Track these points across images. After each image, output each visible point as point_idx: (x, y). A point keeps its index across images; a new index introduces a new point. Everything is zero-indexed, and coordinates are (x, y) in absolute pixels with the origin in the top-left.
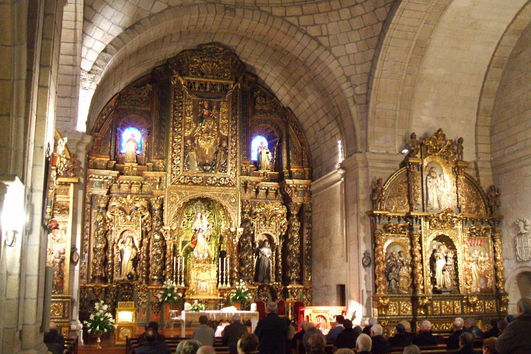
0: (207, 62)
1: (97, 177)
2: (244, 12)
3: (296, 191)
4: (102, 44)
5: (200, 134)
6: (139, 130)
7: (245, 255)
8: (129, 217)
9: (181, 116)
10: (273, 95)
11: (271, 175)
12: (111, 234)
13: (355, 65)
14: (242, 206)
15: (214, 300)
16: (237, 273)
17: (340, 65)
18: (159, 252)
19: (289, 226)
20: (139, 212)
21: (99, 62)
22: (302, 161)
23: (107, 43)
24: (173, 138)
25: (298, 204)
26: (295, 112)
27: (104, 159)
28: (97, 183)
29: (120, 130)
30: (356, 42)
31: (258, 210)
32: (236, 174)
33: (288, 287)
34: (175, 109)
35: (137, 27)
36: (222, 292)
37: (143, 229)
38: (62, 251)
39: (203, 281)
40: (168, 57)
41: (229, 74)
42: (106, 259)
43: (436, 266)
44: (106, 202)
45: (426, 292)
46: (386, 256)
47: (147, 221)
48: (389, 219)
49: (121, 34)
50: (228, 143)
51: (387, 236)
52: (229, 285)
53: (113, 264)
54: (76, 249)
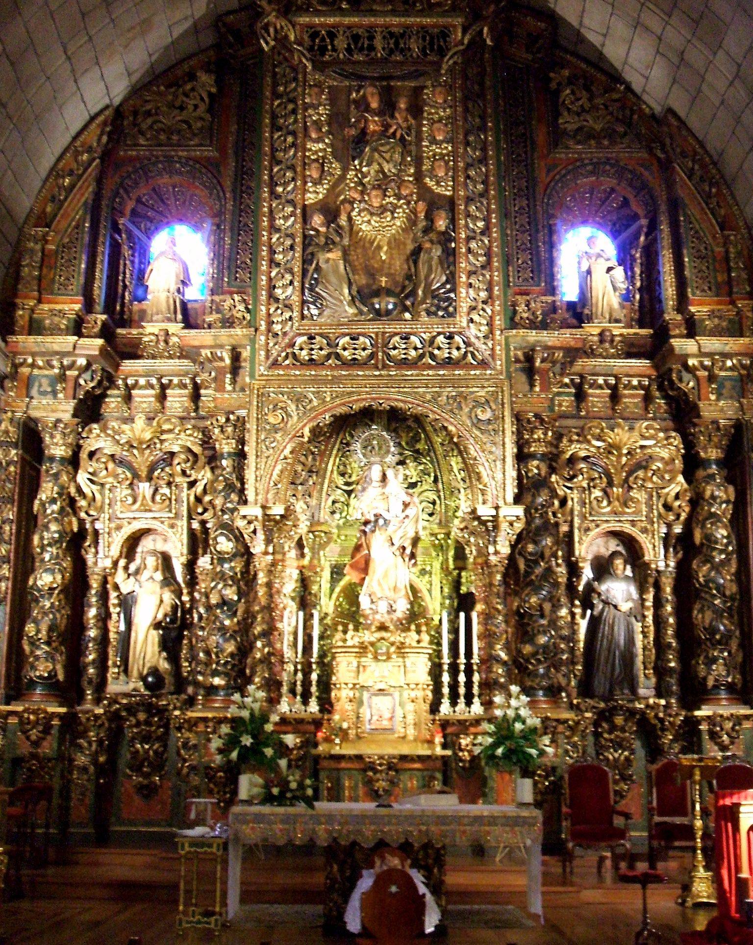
3: (712, 378)
5: (357, 196)
8: (145, 488)
9: (294, 145)
10: (614, 77)
12: (96, 543)
14: (519, 434)
15: (420, 758)
18: (231, 594)
19: (696, 502)
20: (178, 468)
22: (729, 282)
24: (272, 219)
26: (694, 122)
27: (66, 307)
28: (45, 382)
32: (490, 324)
33: (697, 713)
37: (196, 525)
42: (77, 624)
43: (434, 811)
47: (207, 498)
50: (453, 221)
52: (477, 708)
53: (103, 641)
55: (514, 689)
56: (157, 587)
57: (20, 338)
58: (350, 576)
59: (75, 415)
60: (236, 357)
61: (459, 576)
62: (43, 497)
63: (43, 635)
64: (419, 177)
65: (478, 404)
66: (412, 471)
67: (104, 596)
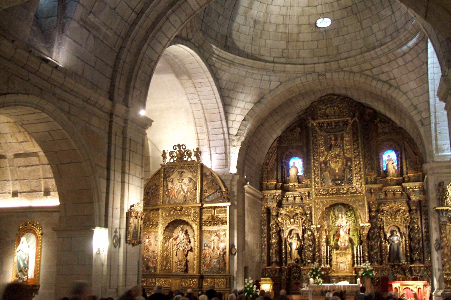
2: (332, 75)
3: (413, 191)
7: (373, 243)
8: (292, 220)
10: (390, 120)
11: (397, 180)
13: (418, 96)
15: (350, 276)
17: (408, 99)
18: (311, 243)
21: (241, 128)
23: (245, 115)
24: (314, 164)
29: (286, 162)
30: (415, 80)
34: (313, 144)
35: (262, 101)
37: (303, 228)
38: (224, 248)
39: (341, 263)
42: (281, 249)
44: (276, 211)
53: (286, 252)
54: (234, 246)
56: (296, 241)
57: (265, 191)
58: (336, 238)
59: (277, 206)
62: (272, 224)
63: (274, 252)
64: (343, 153)
65: (360, 201)
66: (349, 214)
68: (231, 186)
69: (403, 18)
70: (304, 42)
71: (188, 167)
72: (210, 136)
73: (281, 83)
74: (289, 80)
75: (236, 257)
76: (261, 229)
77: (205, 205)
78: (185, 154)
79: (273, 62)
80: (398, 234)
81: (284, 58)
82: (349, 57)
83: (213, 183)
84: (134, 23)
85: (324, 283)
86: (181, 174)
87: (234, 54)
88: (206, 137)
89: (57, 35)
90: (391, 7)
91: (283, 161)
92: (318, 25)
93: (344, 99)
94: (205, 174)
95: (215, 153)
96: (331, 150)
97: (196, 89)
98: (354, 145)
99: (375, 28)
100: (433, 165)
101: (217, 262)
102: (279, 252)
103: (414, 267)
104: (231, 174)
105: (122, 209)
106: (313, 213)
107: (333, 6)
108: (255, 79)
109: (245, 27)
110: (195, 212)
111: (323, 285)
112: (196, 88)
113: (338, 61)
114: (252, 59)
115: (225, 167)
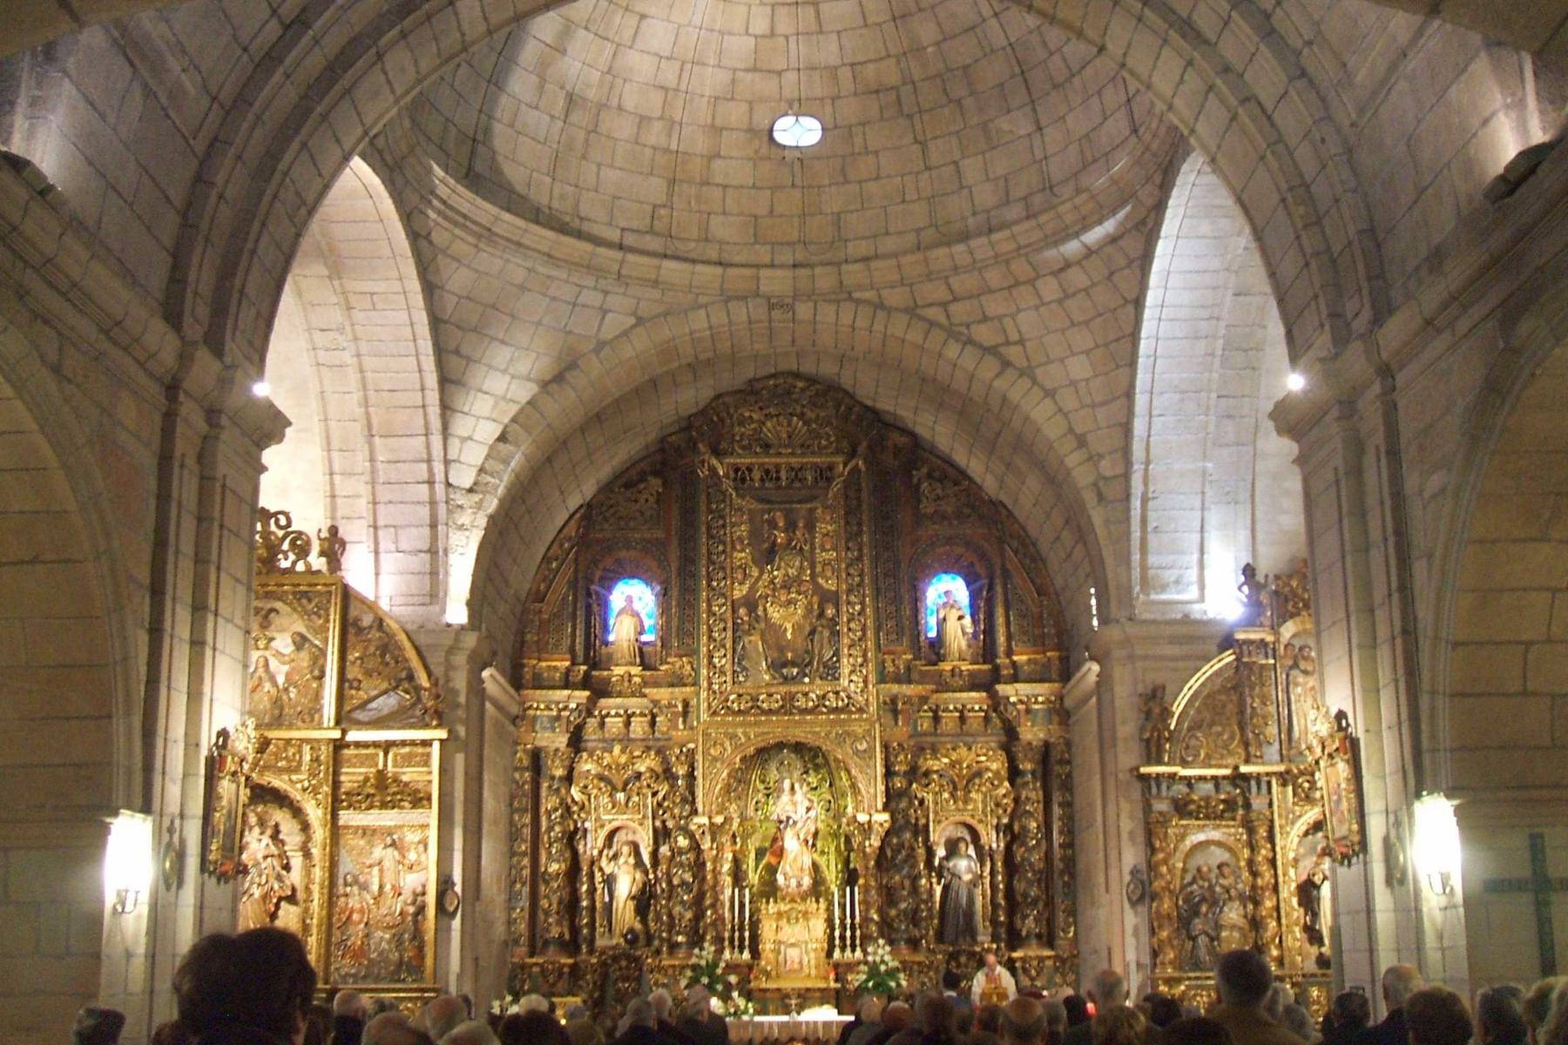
0: (777, 416)
1: (542, 706)
2: (815, 308)
3: (1028, 711)
4: (494, 425)
6: (647, 584)
7: (897, 878)
8: (621, 796)
9: (724, 551)
10: (963, 474)
11: (971, 674)
12: (585, 837)
13: (1093, 406)
15: (819, 990)
16: (877, 923)
17: (1060, 410)
18: (688, 877)
23: (506, 421)
24: (709, 606)
25: (1034, 743)
27: (558, 664)
28: (545, 719)
29: (603, 591)
30: (1087, 352)
31: (934, 764)
34: (710, 536)
35: (568, 376)
36: (841, 970)
37: (658, 823)
38: (419, 889)
39: (793, 945)
40: (684, 413)
41: (833, 439)
42: (575, 898)
44: (567, 763)
45: (1287, 965)
46: (1182, 878)
47: (666, 804)
48: (1190, 785)
49: (534, 396)
51: (1185, 827)
52: (858, 954)
53: (592, 908)
54: (453, 884)
55: (881, 942)
60: (686, 704)
61: (849, 856)
63: (555, 906)
64: (813, 576)
66: (813, 779)
67: (591, 876)
68: (447, 671)
69: (1073, 150)
70: (725, 187)
71: (294, 593)
72: (379, 488)
73: (640, 321)
74: (666, 314)
75: (456, 923)
76: (511, 823)
77: (353, 735)
78: (286, 546)
79: (621, 247)
80: (971, 851)
81: (657, 234)
82: (877, 256)
83: (383, 655)
84: (271, 58)
85: (758, 1012)
86: (266, 617)
87: (495, 204)
88: (364, 490)
89: (26, 65)
90: (1034, 110)
91: (593, 587)
92: (780, 137)
93: (828, 392)
94: (357, 620)
95: (393, 547)
96: (771, 562)
97: (350, 317)
98: (848, 549)
99: (972, 169)
100: (1131, 630)
101: (389, 942)
102: (571, 906)
103: (1023, 960)
104: (449, 625)
105: (192, 744)
106: (698, 773)
107: (836, 77)
108: (554, 299)
109: (537, 113)
110: (316, 760)
111: (757, 1019)
112: (349, 308)
113: (839, 264)
114: (552, 228)
115: (427, 600)
